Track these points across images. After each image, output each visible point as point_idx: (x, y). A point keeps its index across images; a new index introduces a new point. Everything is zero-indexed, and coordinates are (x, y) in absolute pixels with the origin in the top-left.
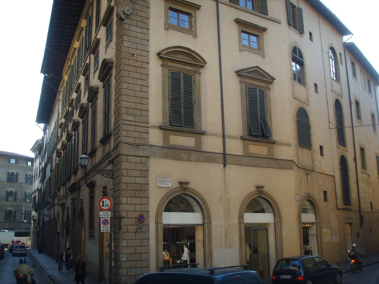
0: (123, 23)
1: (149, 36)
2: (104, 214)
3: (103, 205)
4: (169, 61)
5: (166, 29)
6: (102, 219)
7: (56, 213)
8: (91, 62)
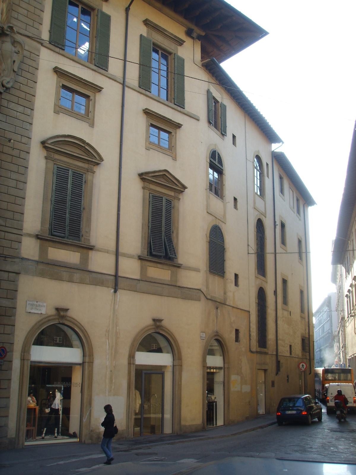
4: (55, 153)
5: (56, 112)
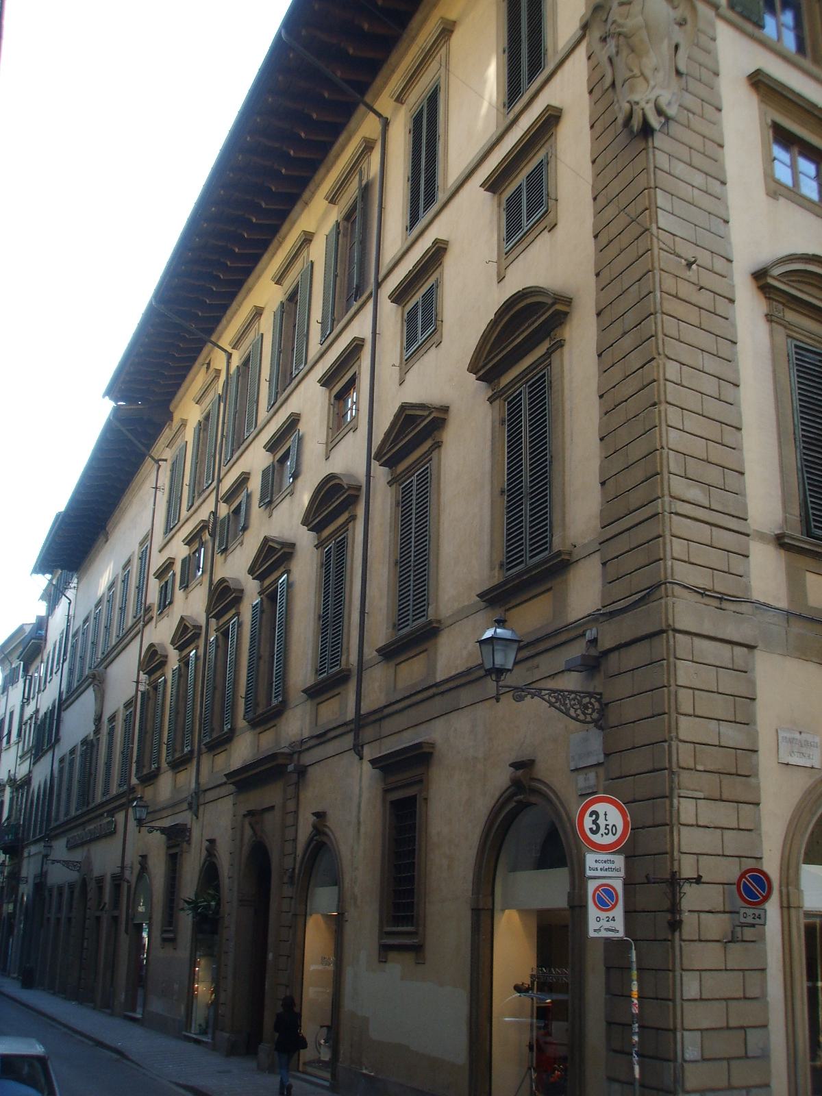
0: (650, 144)
1: (727, 208)
2: (599, 866)
3: (594, 828)
4: (788, 307)
6: (592, 886)
7: (132, 858)
8: (377, 332)
